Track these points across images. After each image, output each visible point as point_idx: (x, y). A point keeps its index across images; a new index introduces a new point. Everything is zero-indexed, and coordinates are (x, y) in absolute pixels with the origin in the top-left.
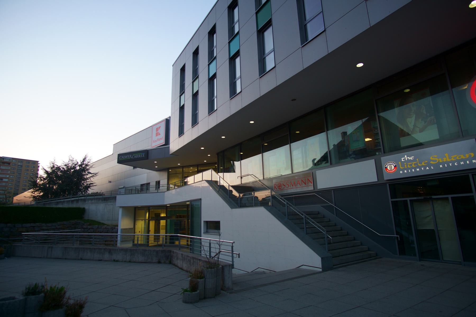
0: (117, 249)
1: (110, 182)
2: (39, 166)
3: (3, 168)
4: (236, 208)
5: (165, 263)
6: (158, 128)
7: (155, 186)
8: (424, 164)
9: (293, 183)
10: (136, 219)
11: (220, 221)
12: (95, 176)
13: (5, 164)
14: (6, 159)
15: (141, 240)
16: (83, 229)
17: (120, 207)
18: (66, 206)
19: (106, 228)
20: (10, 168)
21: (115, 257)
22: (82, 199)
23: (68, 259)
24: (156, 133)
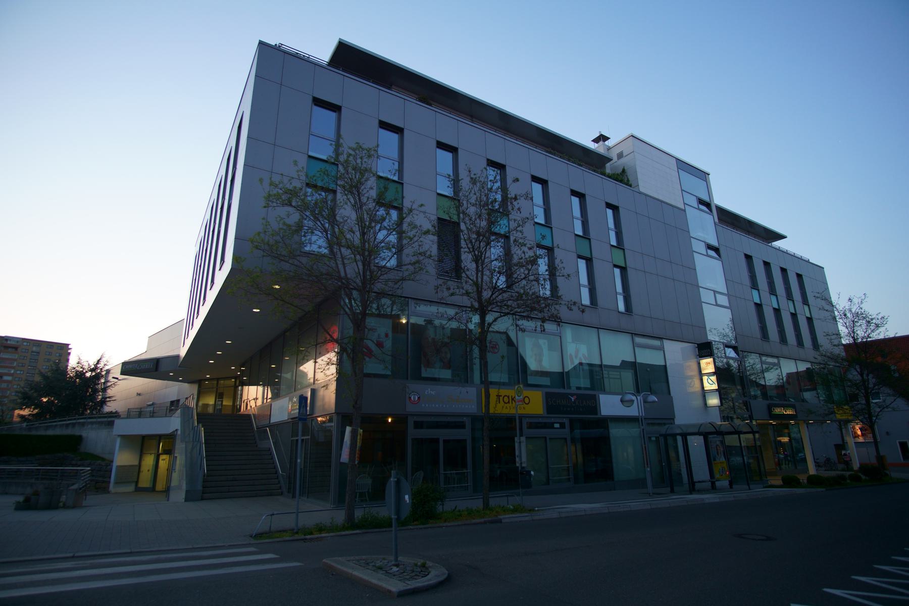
2: (69, 354)
3: (3, 356)
12: (113, 386)
13: (10, 349)
14: (10, 340)
17: (119, 436)
18: (58, 432)
20: (17, 356)
22: (80, 423)
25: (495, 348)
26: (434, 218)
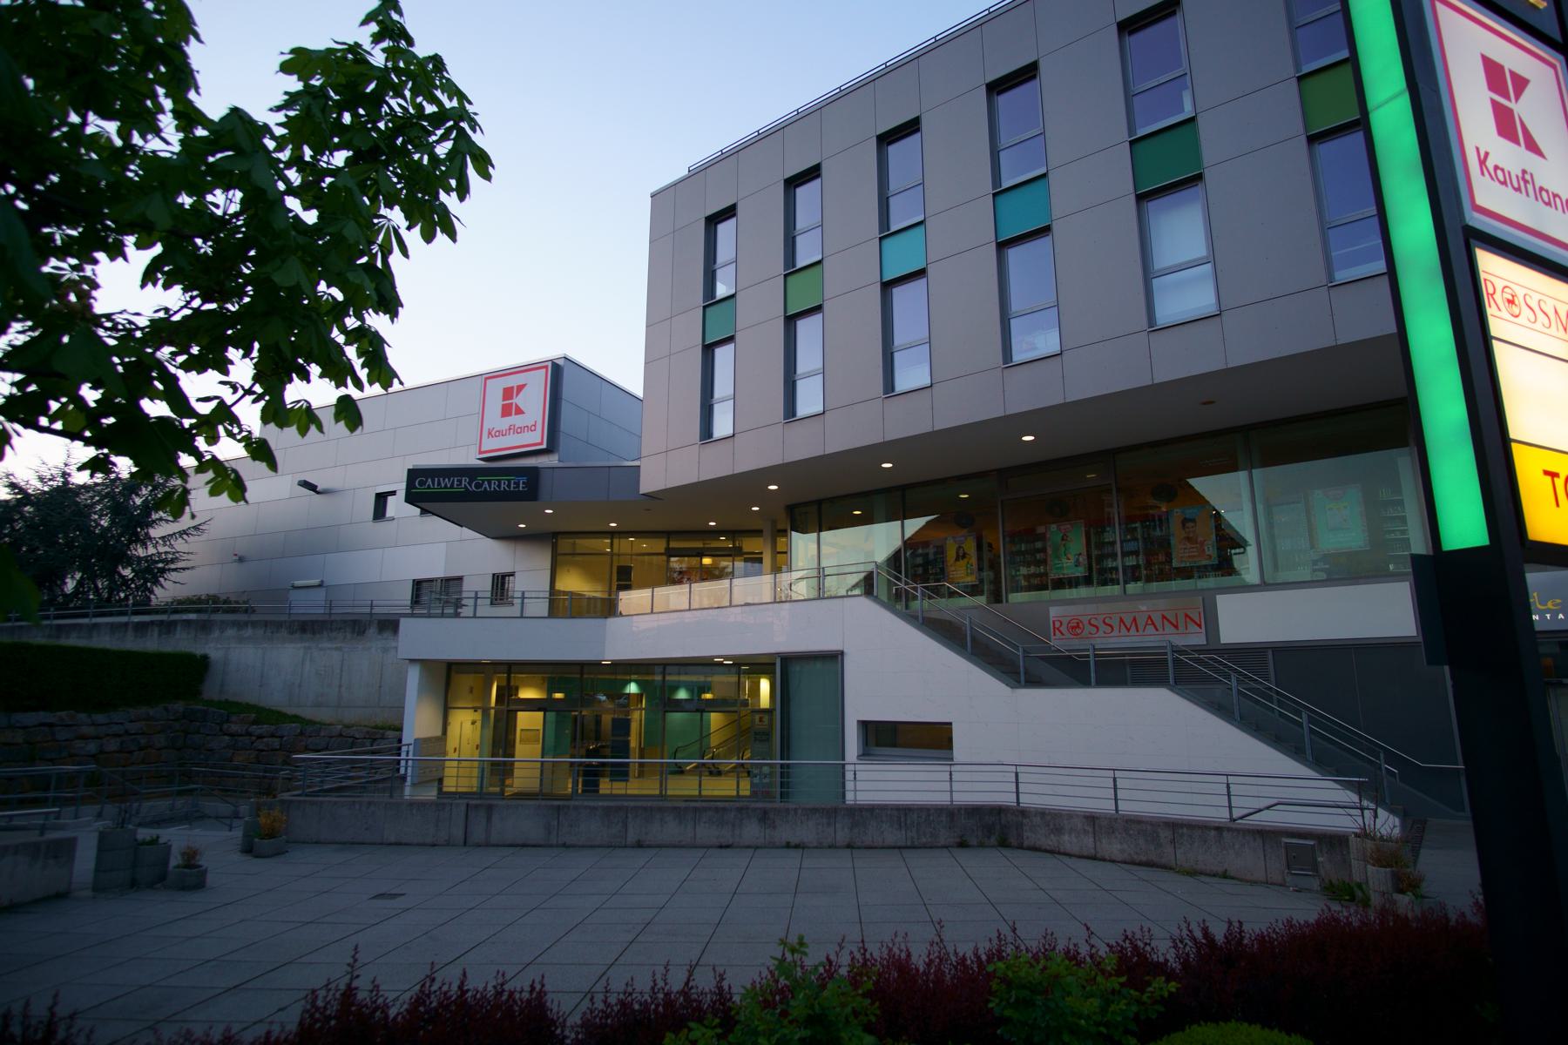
0: (796, 810)
1: (241, 560)
4: (1017, 688)
5: (981, 845)
6: (512, 388)
7: (489, 595)
8: (1553, 605)
9: (1128, 621)
10: (727, 714)
11: (950, 724)
15: (457, 777)
16: (227, 738)
18: (104, 642)
19: (341, 735)
21: (785, 833)
23: (573, 846)
24: (504, 406)
25: (1078, 627)
26: (1243, 572)
